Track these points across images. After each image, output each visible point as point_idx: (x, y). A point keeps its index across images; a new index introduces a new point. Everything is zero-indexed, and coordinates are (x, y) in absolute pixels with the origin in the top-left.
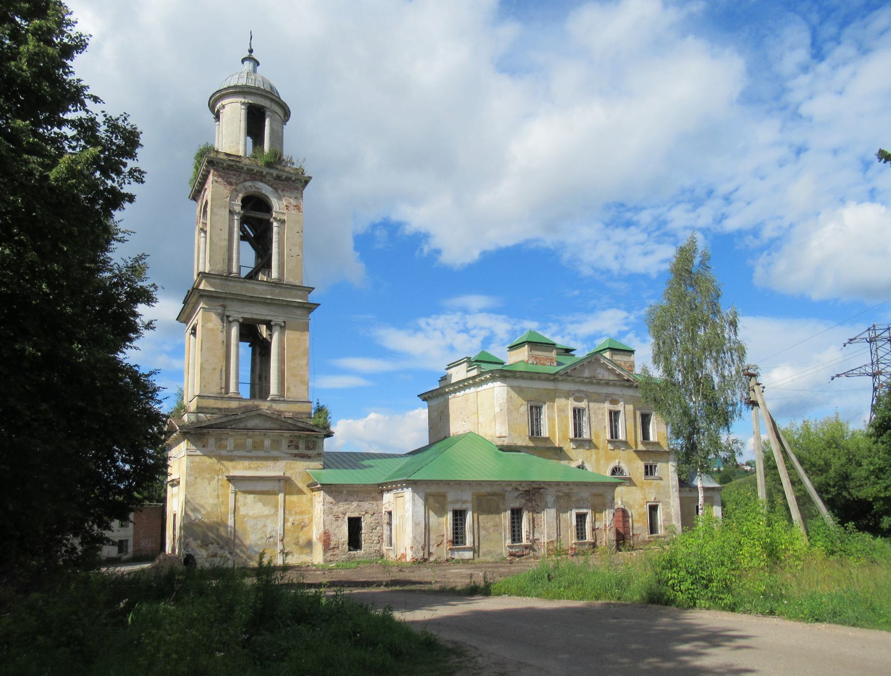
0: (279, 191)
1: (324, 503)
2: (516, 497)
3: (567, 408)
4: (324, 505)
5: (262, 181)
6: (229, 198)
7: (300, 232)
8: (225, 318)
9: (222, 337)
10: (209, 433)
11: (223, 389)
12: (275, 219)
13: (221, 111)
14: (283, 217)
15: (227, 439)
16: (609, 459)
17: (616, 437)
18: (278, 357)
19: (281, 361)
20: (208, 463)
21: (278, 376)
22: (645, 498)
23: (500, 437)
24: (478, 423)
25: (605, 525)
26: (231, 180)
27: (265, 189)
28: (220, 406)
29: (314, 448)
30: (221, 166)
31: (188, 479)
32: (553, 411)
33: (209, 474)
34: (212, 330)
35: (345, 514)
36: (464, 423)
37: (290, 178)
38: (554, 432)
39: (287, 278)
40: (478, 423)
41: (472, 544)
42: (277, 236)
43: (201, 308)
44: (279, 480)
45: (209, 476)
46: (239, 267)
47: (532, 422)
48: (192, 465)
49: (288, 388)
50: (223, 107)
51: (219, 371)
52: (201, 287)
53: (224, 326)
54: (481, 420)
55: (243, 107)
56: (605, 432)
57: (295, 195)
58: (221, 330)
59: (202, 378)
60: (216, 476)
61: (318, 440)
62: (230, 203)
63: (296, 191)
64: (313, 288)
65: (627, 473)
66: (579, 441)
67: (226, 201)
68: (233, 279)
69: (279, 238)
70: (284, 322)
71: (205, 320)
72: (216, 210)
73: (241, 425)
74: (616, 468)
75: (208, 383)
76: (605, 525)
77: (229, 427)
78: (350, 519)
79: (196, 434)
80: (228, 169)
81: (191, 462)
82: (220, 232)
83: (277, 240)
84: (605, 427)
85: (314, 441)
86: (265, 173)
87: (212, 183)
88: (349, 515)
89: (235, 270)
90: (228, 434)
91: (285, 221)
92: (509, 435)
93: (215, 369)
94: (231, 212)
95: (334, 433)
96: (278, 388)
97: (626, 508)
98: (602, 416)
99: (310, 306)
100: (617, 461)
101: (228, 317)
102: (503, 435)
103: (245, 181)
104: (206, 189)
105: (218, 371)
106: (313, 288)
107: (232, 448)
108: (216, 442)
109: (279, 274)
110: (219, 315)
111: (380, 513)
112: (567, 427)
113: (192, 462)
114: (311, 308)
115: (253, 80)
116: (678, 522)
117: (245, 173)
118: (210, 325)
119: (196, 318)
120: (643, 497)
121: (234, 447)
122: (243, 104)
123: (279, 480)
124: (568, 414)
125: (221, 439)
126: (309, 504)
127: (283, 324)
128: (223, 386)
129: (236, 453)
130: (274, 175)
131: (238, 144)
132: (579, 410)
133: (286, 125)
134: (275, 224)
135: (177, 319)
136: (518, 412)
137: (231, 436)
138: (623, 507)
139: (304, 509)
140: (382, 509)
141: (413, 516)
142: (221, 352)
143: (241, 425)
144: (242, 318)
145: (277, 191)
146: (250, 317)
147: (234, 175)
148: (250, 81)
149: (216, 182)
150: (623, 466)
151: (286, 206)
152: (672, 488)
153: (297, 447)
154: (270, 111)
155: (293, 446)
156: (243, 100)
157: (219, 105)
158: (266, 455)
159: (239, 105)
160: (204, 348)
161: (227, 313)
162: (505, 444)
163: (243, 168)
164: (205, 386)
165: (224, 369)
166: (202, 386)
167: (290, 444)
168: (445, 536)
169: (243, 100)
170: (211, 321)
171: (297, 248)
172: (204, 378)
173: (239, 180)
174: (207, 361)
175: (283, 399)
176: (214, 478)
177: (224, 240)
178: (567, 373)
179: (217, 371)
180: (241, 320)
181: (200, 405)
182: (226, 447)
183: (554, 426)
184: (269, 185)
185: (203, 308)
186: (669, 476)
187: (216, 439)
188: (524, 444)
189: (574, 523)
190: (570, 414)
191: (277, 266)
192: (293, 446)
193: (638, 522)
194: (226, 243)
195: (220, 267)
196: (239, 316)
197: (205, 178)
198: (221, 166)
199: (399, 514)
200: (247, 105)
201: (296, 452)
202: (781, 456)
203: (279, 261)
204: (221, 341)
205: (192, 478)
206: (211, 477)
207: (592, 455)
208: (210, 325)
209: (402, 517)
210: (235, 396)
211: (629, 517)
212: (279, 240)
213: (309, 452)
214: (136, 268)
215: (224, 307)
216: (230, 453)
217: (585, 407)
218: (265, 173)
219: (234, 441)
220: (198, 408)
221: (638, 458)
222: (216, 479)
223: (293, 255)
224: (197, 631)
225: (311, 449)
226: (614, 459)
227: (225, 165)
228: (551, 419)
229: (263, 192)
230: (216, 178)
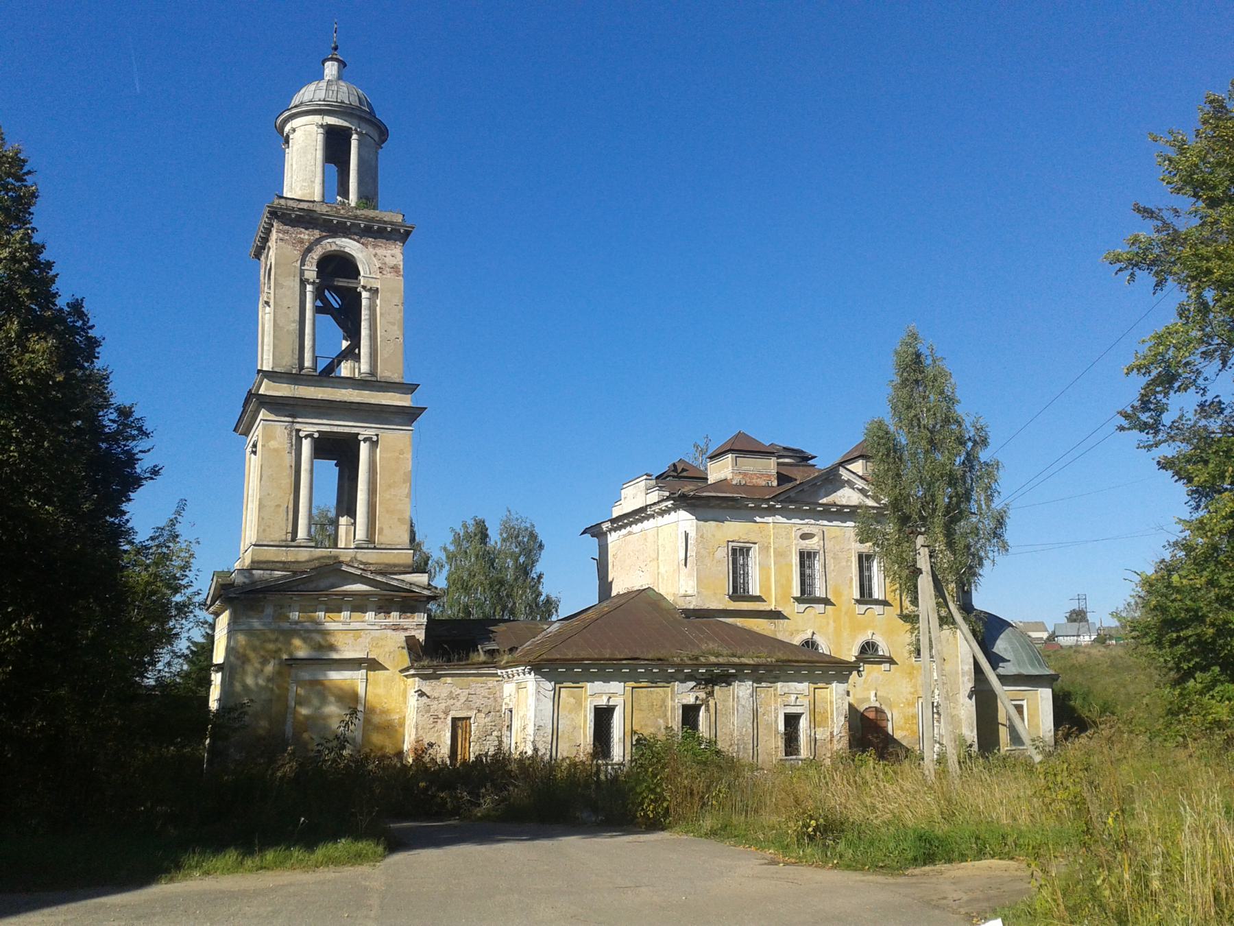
2: (693, 688)
3: (791, 552)
6: (299, 262)
8: (294, 433)
11: (290, 535)
12: (364, 287)
13: (291, 136)
14: (377, 285)
16: (856, 628)
17: (870, 595)
19: (372, 491)
22: (916, 691)
23: (685, 596)
24: (658, 573)
25: (832, 733)
26: (302, 236)
27: (349, 246)
28: (284, 559)
32: (768, 556)
34: (276, 450)
35: (446, 713)
38: (769, 589)
39: (381, 372)
40: (658, 573)
41: (622, 759)
42: (367, 312)
43: (261, 420)
46: (315, 359)
47: (735, 572)
49: (381, 530)
50: (294, 130)
51: (285, 509)
52: (261, 392)
53: (292, 446)
54: (662, 570)
56: (851, 587)
58: (288, 450)
62: (301, 269)
64: (419, 385)
65: (883, 650)
66: (806, 597)
67: (295, 266)
68: (305, 377)
69: (370, 315)
70: (377, 435)
71: (268, 436)
72: (281, 280)
73: (311, 586)
74: (867, 643)
75: (269, 527)
76: (832, 733)
78: (454, 720)
82: (287, 311)
83: (367, 317)
84: (852, 579)
86: (348, 224)
88: (453, 714)
89: (308, 363)
91: (377, 289)
92: (698, 593)
93: (278, 506)
94: (303, 282)
97: (883, 707)
98: (847, 561)
99: (412, 411)
100: (869, 633)
102: (689, 593)
104: (269, 248)
106: (419, 385)
108: (275, 611)
109: (371, 366)
111: (498, 711)
112: (789, 580)
114: (414, 414)
115: (335, 92)
116: (972, 731)
118: (273, 444)
119: (256, 434)
120: (912, 690)
124: (791, 561)
125: (282, 607)
126: (401, 699)
128: (290, 530)
130: (362, 226)
131: (313, 182)
132: (809, 554)
133: (382, 148)
134: (365, 294)
135: (234, 430)
136: (713, 557)
138: (877, 705)
139: (393, 705)
140: (501, 706)
141: (535, 716)
142: (288, 482)
143: (311, 586)
144: (318, 431)
148: (331, 92)
150: (879, 640)
151: (380, 268)
152: (963, 676)
157: (287, 129)
162: (692, 607)
163: (317, 219)
164: (264, 530)
165: (291, 506)
166: (261, 530)
168: (582, 746)
170: (275, 438)
174: (269, 494)
175: (372, 546)
177: (294, 322)
178: (789, 497)
179: (281, 509)
180: (316, 435)
181: (256, 559)
183: (768, 579)
185: (264, 420)
186: (957, 656)
187: (275, 606)
188: (721, 607)
189: (781, 727)
190: (795, 560)
191: (368, 355)
193: (902, 729)
194: (295, 326)
195: (288, 362)
199: (521, 714)
200: (326, 128)
202: (311, 343)
203: (371, 348)
204: (288, 465)
207: (828, 623)
209: (524, 717)
211: (888, 720)
212: (370, 319)
217: (818, 548)
220: (253, 562)
224: (776, 811)
226: (865, 628)
228: (764, 568)
229: (347, 250)
230: (281, 235)
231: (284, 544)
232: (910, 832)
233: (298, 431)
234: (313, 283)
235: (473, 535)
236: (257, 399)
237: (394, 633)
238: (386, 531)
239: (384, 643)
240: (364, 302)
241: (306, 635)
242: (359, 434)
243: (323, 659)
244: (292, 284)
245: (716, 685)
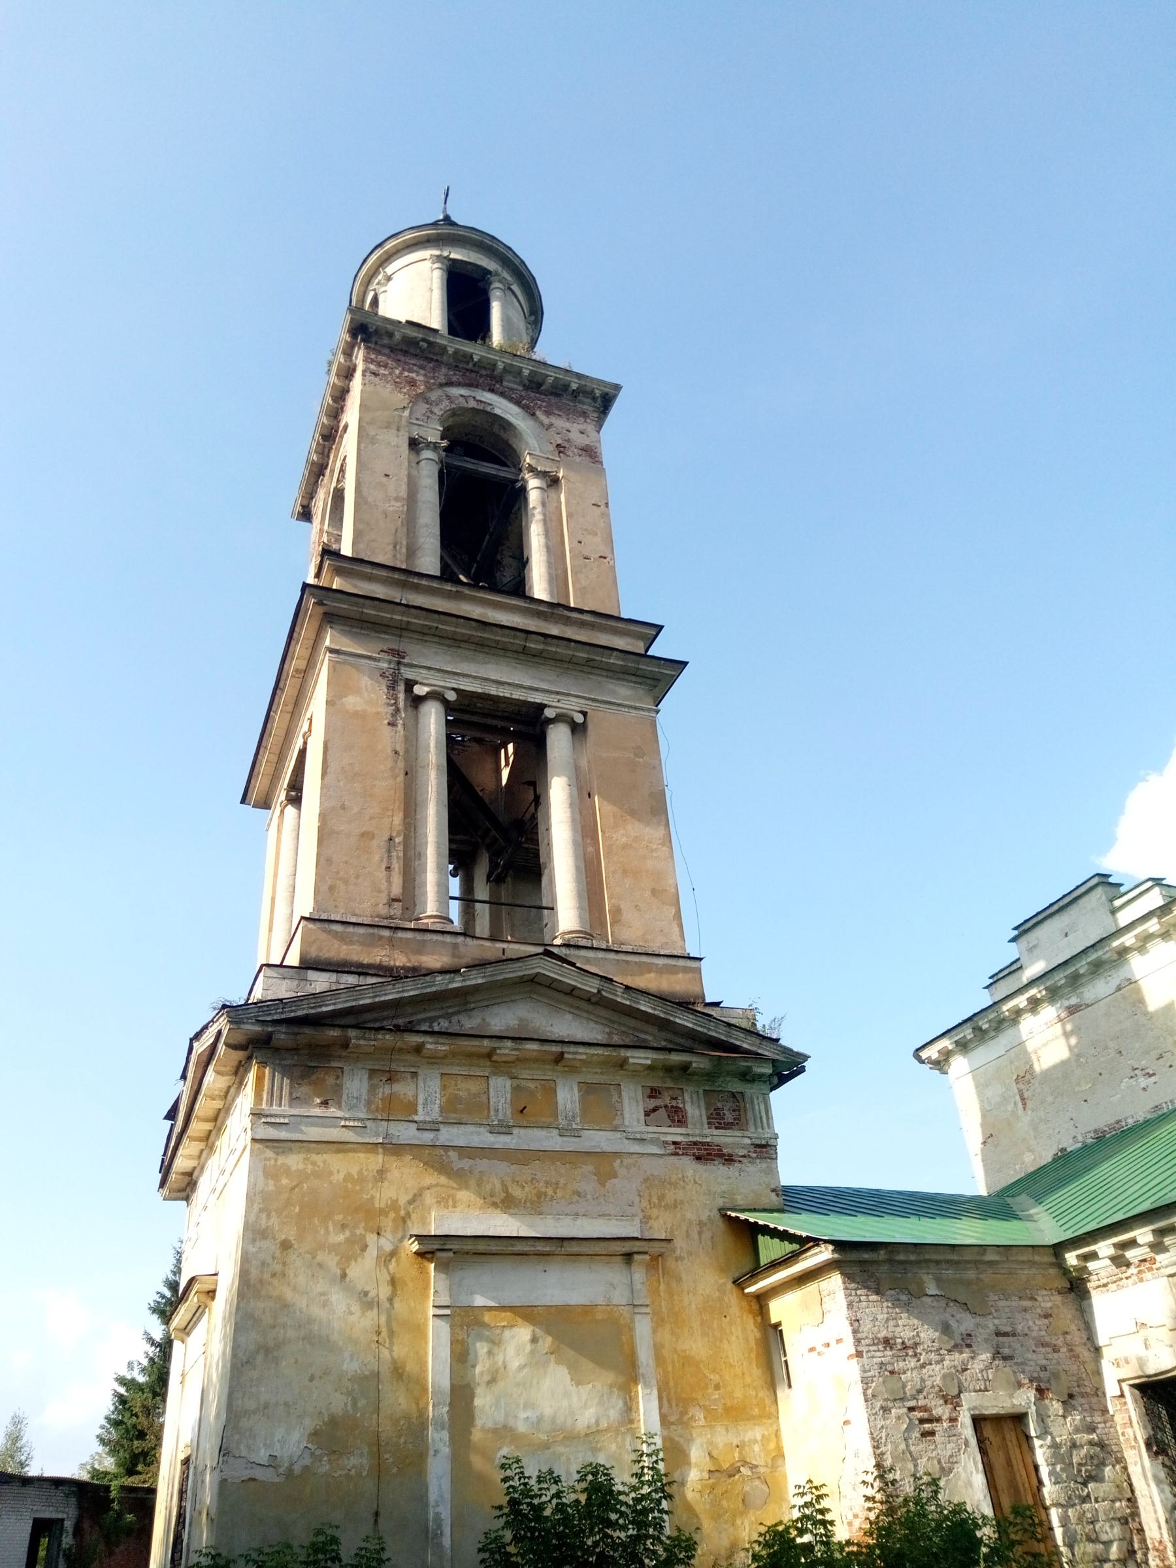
0: (538, 413)
1: (858, 1341)
4: (859, 1354)
5: (492, 391)
7: (602, 504)
8: (401, 687)
9: (389, 739)
10: (345, 1045)
12: (531, 469)
15: (415, 1075)
18: (572, 812)
20: (338, 1178)
21: (577, 868)
29: (738, 1123)
30: (386, 341)
31: (252, 1249)
33: (343, 1226)
35: (953, 1401)
36: (1143, 1082)
37: (566, 387)
44: (628, 1257)
45: (341, 1238)
48: (271, 1186)
49: (616, 911)
55: (437, 265)
57: (581, 427)
58: (389, 718)
59: (324, 861)
60: (371, 1238)
61: (750, 1090)
63: (582, 419)
67: (401, 416)
70: (585, 714)
77: (424, 1027)
79: (295, 1050)
80: (406, 353)
81: (267, 1174)
82: (385, 479)
85: (733, 1095)
86: (500, 366)
87: (364, 375)
88: (970, 1402)
90: (418, 1049)
93: (366, 836)
95: (806, 1058)
96: (580, 908)
101: (410, 685)
103: (450, 384)
105: (379, 843)
107: (435, 1114)
108: (372, 1089)
110: (383, 675)
113: (270, 1174)
117: (449, 366)
118: (352, 702)
121: (442, 1110)
122: (439, 258)
123: (628, 1257)
127: (579, 718)
129: (450, 1135)
130: (526, 373)
137: (435, 1060)
142: (387, 785)
145: (533, 415)
146: (480, 691)
147: (421, 367)
149: (375, 374)
153: (677, 1117)
154: (500, 281)
155: (662, 1112)
156: (437, 252)
158: (570, 1144)
159: (428, 264)
160: (333, 767)
161: (408, 674)
164: (331, 888)
167: (652, 1103)
169: (437, 252)
171: (598, 539)
172: (329, 861)
173: (433, 378)
174: (343, 807)
176: (364, 1248)
177: (397, 499)
179: (375, 843)
181: (313, 953)
182: (412, 1107)
184: (511, 400)
187: (372, 1073)
191: (545, 577)
192: (662, 1112)
196: (449, 686)
197: (348, 373)
198: (386, 341)
201: (675, 1134)
204: (389, 751)
205: (270, 1246)
206: (350, 1242)
208: (352, 702)
210: (438, 927)
213: (727, 1139)
214: (83, 1466)
215: (398, 656)
216: (428, 1137)
218: (500, 366)
219: (444, 1087)
220: (302, 960)
221: (692, 1503)
222: (372, 1253)
223: (586, 554)
225: (728, 1126)
227: (398, 336)
230: (372, 367)
231: (385, 923)
232: (472, 1182)
233: (410, 685)
234: (435, 447)
235: (535, 1199)
236: (319, 603)
237: (700, 1167)
238: (628, 915)
239: (680, 1195)
240: (534, 497)
241: (466, 1164)
242: (545, 706)
243: (336, 1255)
244: (394, 441)
245: (848, 1277)
